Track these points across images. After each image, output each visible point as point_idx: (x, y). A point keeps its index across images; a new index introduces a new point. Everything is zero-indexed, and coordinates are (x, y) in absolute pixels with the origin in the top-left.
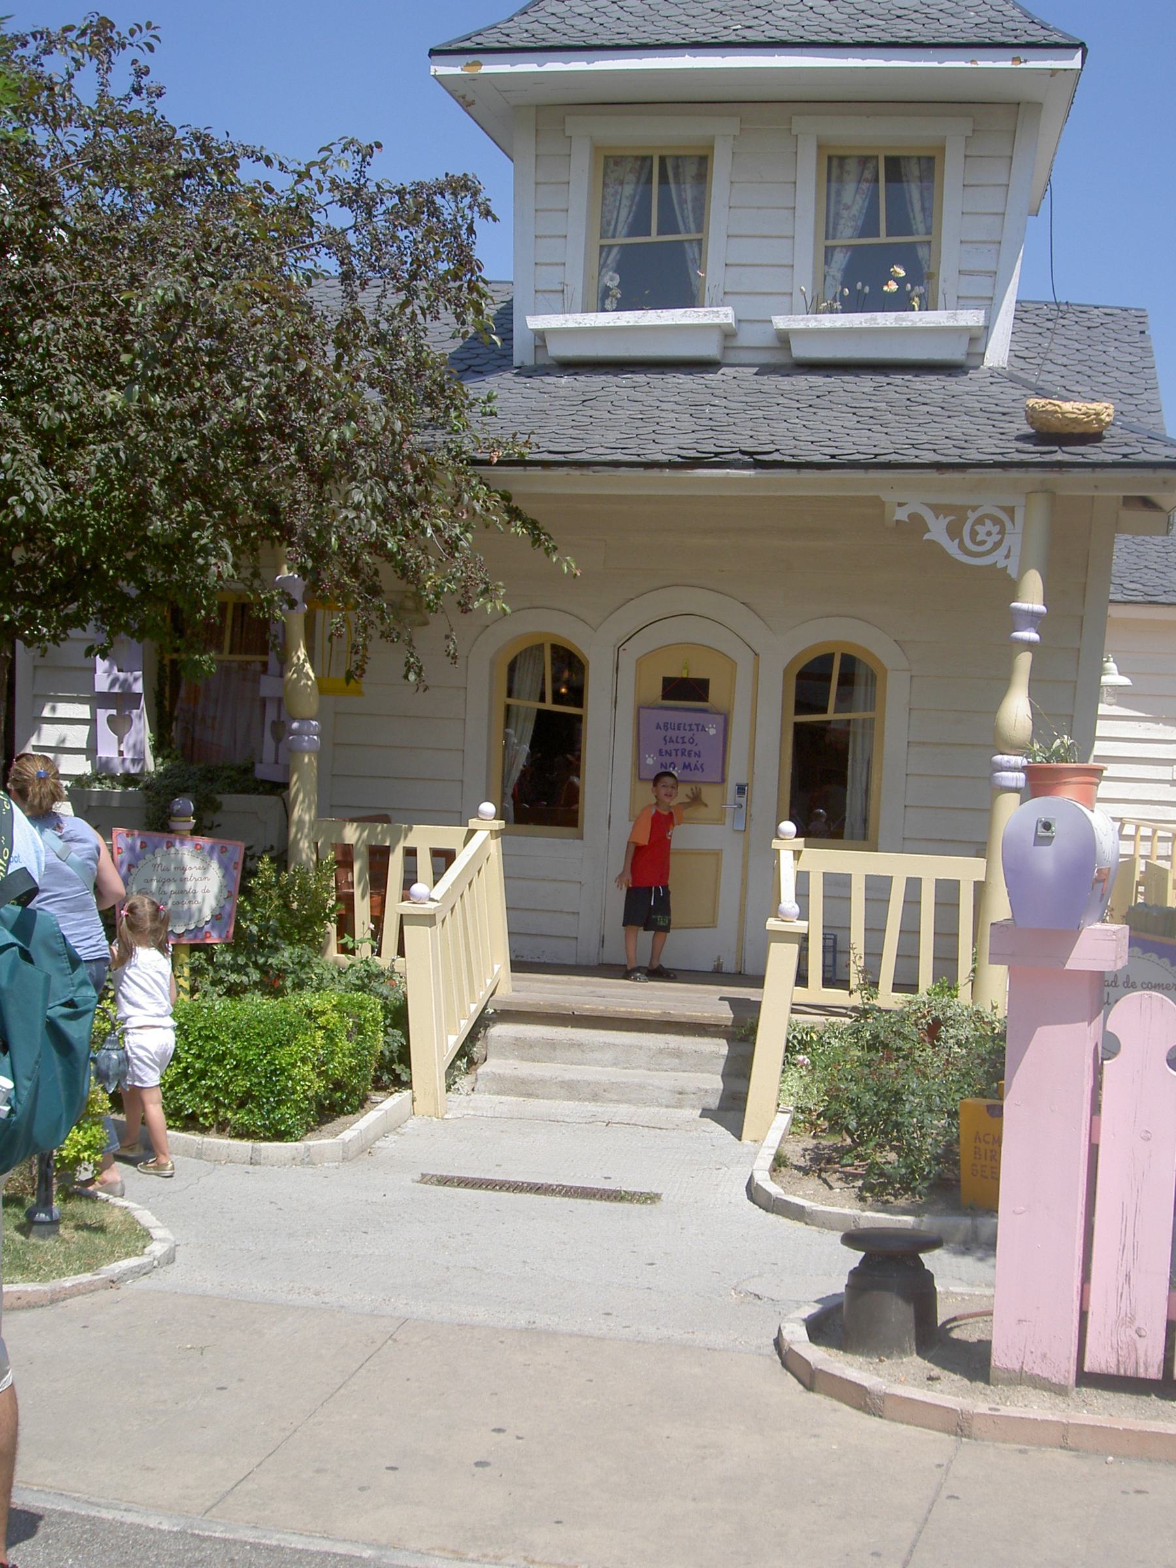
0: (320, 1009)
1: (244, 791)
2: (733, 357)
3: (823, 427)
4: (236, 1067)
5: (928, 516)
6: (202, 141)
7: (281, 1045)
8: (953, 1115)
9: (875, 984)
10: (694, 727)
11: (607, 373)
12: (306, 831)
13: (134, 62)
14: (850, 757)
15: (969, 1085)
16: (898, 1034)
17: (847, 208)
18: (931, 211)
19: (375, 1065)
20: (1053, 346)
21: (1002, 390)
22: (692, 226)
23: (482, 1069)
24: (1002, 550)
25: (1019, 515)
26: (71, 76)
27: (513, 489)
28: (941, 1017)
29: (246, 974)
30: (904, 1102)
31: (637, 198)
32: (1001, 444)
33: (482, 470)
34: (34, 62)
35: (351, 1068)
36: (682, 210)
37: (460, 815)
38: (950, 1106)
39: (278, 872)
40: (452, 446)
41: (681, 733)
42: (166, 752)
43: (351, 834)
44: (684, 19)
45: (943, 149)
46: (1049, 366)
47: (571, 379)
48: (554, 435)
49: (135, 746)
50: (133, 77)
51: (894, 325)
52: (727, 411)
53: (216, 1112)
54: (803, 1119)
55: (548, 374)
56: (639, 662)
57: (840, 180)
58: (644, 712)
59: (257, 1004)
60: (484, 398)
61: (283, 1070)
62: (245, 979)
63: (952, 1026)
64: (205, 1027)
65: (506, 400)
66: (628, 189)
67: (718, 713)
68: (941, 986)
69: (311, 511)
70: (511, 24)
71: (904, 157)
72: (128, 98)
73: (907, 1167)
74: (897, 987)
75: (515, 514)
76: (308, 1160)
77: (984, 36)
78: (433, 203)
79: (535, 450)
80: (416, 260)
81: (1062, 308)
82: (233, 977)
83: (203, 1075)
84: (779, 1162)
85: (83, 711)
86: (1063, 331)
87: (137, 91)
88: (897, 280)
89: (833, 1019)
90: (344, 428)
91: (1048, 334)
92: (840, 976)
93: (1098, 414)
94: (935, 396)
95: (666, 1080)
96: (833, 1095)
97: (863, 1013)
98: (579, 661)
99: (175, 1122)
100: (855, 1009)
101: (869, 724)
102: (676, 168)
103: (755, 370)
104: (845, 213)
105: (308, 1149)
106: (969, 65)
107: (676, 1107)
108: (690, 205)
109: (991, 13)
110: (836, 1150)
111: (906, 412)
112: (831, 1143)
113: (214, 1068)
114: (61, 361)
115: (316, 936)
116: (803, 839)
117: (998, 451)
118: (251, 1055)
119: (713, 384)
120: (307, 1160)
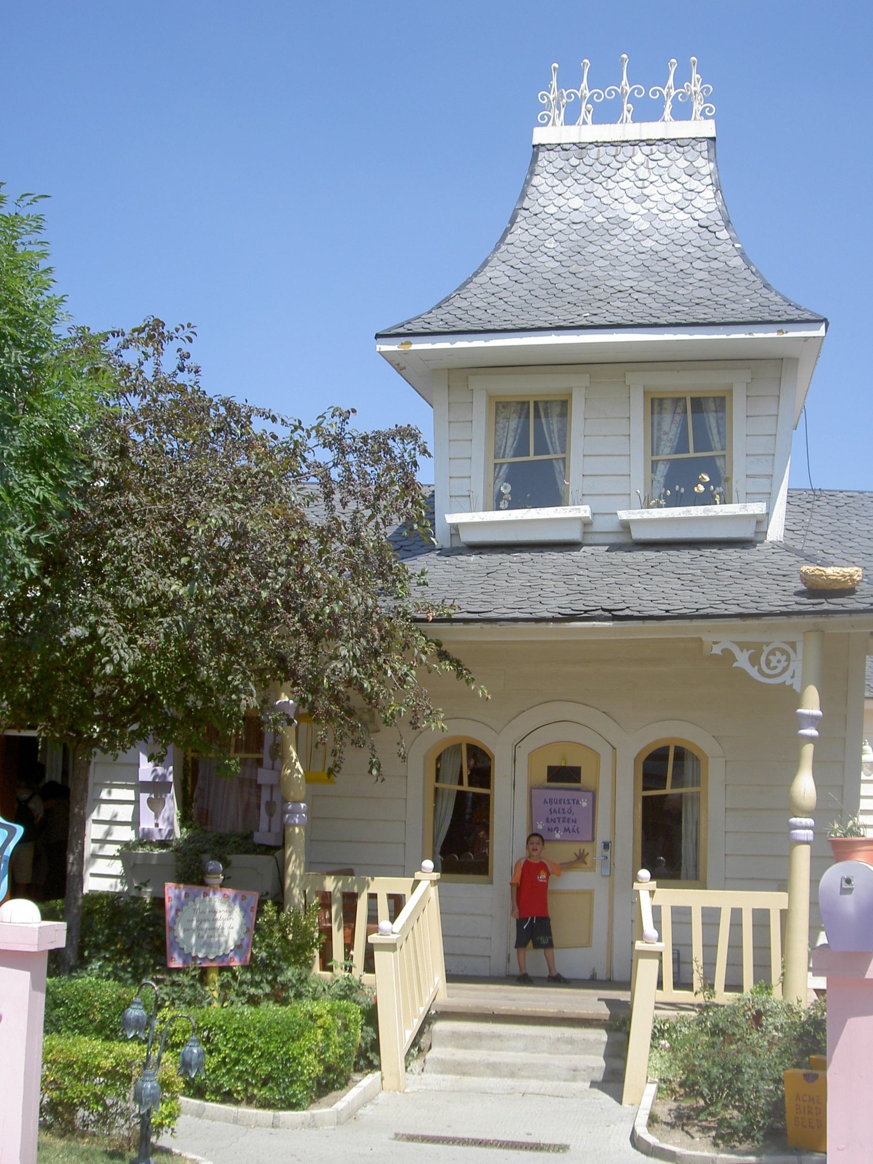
0: (319, 1013)
1: (246, 852)
2: (590, 539)
3: (658, 589)
4: (261, 1056)
5: (736, 650)
6: (227, 404)
7: (293, 1040)
8: (778, 1081)
9: (712, 986)
10: (571, 802)
11: (502, 553)
12: (298, 882)
13: (179, 350)
14: (683, 820)
15: (788, 1060)
16: (732, 1022)
17: (666, 433)
18: (725, 433)
19: (355, 1054)
20: (812, 521)
21: (781, 557)
22: (558, 449)
23: (429, 1055)
24: (788, 673)
25: (799, 647)
26: (141, 364)
27: (442, 638)
28: (762, 1010)
29: (261, 988)
30: (743, 1073)
31: (519, 431)
32: (785, 598)
33: (421, 625)
34: (116, 354)
35: (340, 1056)
36: (551, 438)
37: (407, 869)
38: (776, 1075)
39: (278, 912)
40: (400, 609)
41: (562, 806)
42: (189, 823)
43: (330, 884)
44: (550, 309)
45: (731, 391)
46: (812, 537)
47: (477, 557)
48: (469, 599)
49: (168, 819)
50: (179, 360)
51: (703, 515)
52: (589, 579)
53: (246, 1090)
54: (665, 1087)
55: (461, 554)
56: (530, 755)
57: (660, 413)
58: (534, 791)
59: (270, 1010)
60: (419, 573)
61: (295, 1059)
62: (260, 991)
63: (770, 1016)
64: (238, 1028)
65: (433, 573)
66: (513, 424)
67: (588, 791)
68: (760, 987)
69: (310, 661)
70: (430, 315)
71: (704, 398)
72: (175, 374)
73: (748, 1120)
74: (728, 988)
75: (443, 655)
76: (313, 1124)
77: (757, 316)
78: (387, 444)
79: (458, 611)
80: (378, 487)
81: (817, 493)
82: (253, 991)
83: (237, 1062)
84: (653, 1119)
85: (130, 795)
86: (819, 510)
87: (182, 369)
88: (704, 484)
89: (683, 1013)
90: (334, 605)
91: (809, 512)
92: (393, 901)
93: (851, 576)
94: (734, 564)
95: (563, 1060)
96: (690, 1069)
97: (704, 1008)
98: (481, 750)
99: (216, 1097)
100: (699, 1005)
101: (696, 798)
102: (546, 410)
103: (607, 548)
104: (665, 437)
105: (313, 1116)
106: (748, 336)
107: (572, 1081)
108: (556, 434)
109: (761, 300)
110: (693, 1109)
111: (715, 577)
112: (688, 1105)
113: (245, 1058)
114: (140, 560)
115: (307, 959)
116: (655, 883)
117: (783, 603)
118: (272, 1047)
119: (578, 559)
120: (312, 1124)
